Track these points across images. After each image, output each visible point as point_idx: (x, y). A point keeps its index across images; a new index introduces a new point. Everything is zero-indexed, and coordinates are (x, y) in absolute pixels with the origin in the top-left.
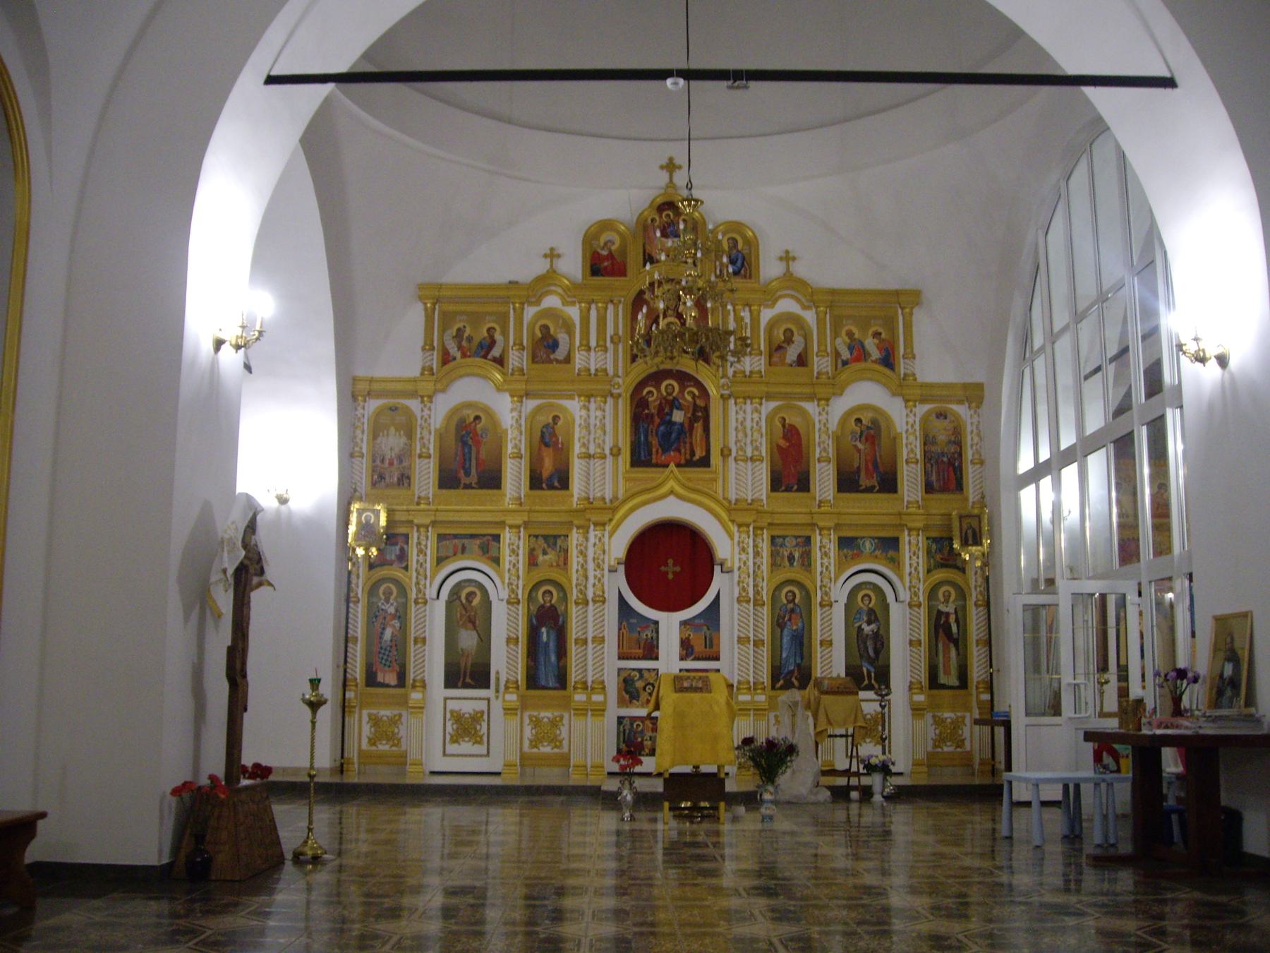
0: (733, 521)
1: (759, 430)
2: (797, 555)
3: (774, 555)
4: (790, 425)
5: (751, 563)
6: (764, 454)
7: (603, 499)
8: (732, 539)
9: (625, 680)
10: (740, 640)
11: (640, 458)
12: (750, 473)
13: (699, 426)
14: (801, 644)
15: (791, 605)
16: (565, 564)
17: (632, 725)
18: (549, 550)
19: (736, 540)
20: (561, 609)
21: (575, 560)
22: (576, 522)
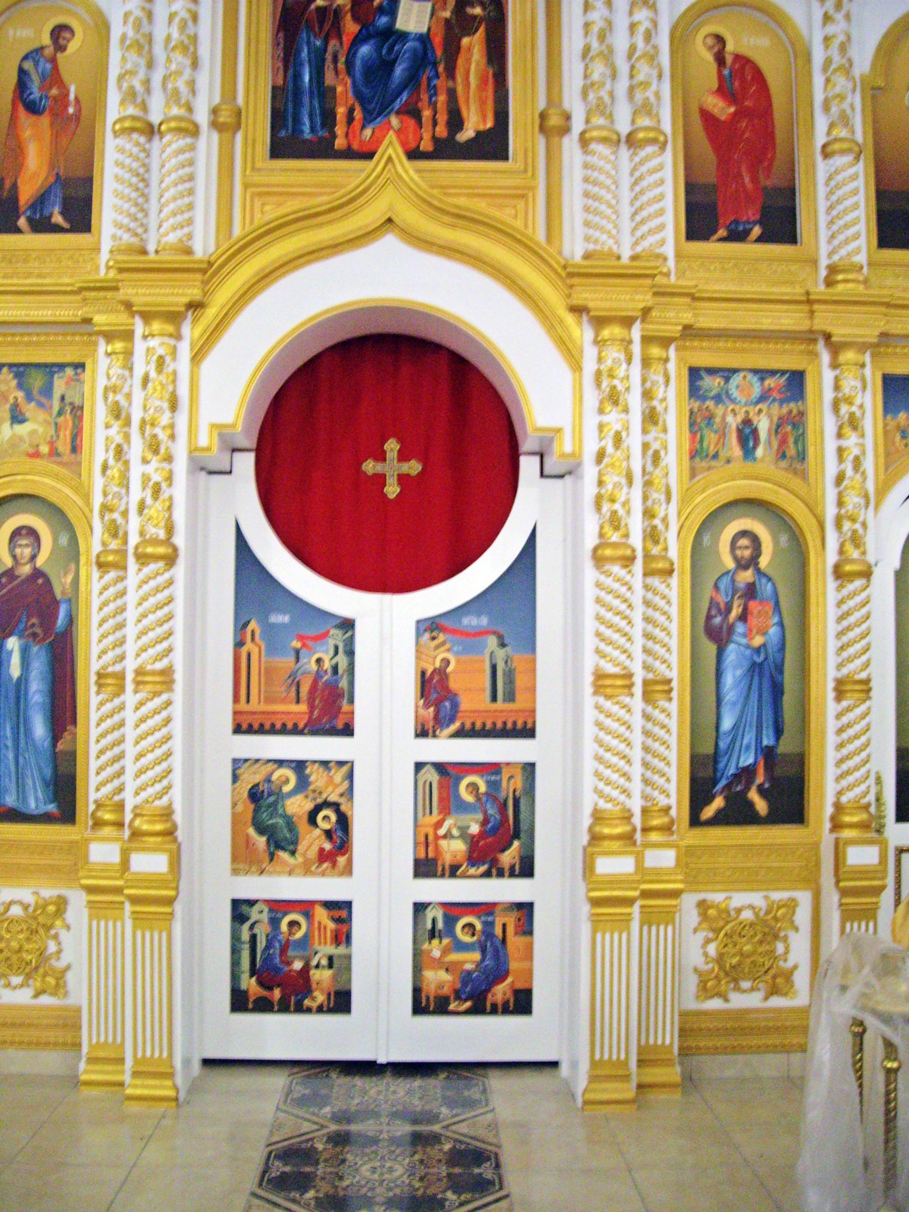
0: (578, 310)
1: (652, 57)
2: (763, 426)
3: (697, 424)
4: (738, 57)
5: (634, 440)
6: (667, 126)
7: (627, 816)
8: (576, 366)
9: (255, 795)
10: (602, 682)
11: (299, 130)
12: (626, 181)
13: (474, 45)
14: (777, 691)
15: (747, 576)
16: (75, 448)
17: (275, 922)
18: (30, 409)
19: (590, 365)
20: (61, 584)
21: (100, 434)
22: (100, 319)
